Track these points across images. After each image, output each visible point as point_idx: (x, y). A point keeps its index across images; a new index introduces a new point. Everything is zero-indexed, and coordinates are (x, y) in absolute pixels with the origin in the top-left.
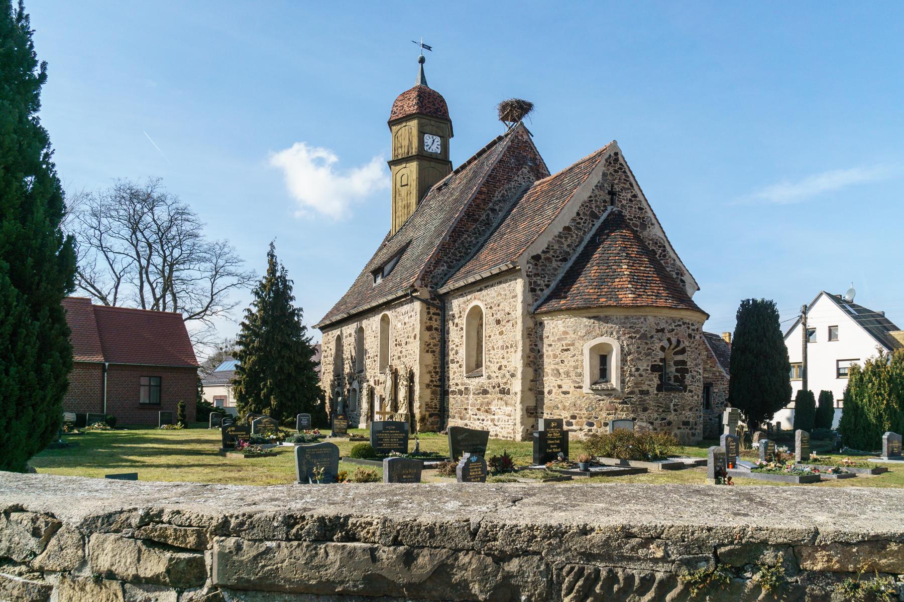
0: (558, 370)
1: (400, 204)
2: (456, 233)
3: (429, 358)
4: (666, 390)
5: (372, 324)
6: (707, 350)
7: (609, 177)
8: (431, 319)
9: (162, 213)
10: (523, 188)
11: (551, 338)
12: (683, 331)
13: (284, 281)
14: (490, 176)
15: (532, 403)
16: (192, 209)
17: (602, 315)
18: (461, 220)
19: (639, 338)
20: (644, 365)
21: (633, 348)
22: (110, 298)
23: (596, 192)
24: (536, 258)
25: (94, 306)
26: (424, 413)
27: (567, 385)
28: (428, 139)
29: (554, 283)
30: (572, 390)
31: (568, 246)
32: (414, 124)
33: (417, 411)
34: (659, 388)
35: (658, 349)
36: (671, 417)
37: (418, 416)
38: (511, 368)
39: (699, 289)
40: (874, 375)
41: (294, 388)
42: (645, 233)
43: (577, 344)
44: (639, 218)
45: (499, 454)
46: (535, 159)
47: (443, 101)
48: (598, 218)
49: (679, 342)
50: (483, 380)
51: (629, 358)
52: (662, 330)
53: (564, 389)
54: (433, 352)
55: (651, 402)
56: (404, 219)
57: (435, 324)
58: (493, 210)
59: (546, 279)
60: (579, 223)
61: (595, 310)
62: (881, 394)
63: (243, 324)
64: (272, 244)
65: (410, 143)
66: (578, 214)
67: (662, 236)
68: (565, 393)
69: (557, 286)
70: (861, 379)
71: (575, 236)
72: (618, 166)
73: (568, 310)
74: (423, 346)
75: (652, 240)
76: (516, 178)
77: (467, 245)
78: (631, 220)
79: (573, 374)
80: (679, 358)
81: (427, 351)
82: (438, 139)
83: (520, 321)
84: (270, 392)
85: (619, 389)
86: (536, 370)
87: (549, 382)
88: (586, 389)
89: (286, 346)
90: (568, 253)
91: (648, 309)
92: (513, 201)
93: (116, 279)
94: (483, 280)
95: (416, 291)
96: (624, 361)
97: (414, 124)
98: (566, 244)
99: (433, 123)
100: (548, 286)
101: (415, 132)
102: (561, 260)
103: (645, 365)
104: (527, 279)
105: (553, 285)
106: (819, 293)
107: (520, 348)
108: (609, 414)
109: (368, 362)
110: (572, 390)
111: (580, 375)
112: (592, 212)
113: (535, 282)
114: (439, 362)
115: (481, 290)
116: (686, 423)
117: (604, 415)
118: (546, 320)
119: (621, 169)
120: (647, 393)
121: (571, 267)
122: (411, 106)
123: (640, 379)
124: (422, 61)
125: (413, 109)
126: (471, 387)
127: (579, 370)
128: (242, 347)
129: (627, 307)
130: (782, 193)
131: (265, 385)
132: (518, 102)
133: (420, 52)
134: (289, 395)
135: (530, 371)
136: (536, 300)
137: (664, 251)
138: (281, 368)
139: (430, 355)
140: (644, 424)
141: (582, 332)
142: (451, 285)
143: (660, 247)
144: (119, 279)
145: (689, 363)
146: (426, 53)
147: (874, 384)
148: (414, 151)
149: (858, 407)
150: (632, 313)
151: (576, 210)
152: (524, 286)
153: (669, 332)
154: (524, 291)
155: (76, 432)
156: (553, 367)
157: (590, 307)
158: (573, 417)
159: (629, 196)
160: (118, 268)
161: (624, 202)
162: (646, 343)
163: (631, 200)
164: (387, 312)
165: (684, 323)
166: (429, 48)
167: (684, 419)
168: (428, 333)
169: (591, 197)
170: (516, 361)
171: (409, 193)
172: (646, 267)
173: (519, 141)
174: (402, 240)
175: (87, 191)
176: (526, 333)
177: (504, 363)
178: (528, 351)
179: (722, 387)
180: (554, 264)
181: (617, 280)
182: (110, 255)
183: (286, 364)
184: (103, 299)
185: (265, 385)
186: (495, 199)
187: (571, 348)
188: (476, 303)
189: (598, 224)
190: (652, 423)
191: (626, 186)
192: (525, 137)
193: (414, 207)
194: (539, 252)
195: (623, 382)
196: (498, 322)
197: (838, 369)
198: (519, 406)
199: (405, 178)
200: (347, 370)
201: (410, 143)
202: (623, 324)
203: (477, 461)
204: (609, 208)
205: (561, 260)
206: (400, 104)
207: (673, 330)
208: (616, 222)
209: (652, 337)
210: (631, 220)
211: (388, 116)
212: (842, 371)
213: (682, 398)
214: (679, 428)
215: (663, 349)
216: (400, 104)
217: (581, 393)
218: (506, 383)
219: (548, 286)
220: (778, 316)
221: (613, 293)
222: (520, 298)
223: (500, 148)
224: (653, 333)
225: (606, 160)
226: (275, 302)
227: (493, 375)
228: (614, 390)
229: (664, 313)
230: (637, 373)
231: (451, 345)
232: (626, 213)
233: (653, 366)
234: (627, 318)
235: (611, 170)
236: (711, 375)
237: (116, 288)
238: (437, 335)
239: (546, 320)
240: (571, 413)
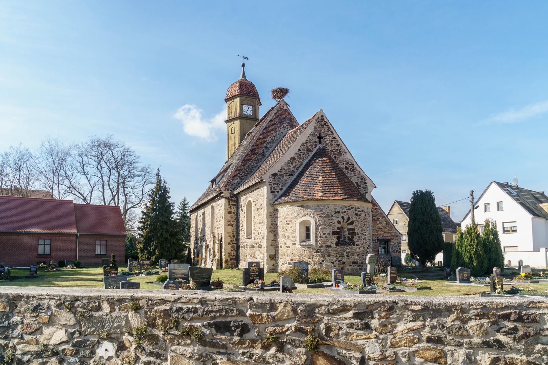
0: (284, 235)
2: (245, 161)
3: (230, 229)
4: (341, 245)
5: (208, 209)
7: (318, 129)
8: (230, 207)
9: (117, 153)
10: (284, 135)
11: (281, 218)
12: (352, 213)
13: (165, 189)
14: (264, 129)
15: (273, 253)
16: (132, 148)
17: (305, 205)
18: (248, 154)
20: (328, 231)
21: (322, 222)
22: (88, 198)
23: (310, 138)
24: (275, 175)
25: (75, 204)
26: (227, 258)
27: (289, 243)
28: (245, 108)
29: (283, 189)
30: (291, 245)
31: (294, 167)
32: (237, 100)
33: (223, 257)
34: (337, 244)
35: (336, 222)
36: (345, 259)
37: (224, 260)
38: (262, 234)
39: (376, 187)
40: (469, 234)
41: (169, 245)
42: (341, 158)
43: (293, 221)
44: (337, 150)
45: (216, 280)
46: (291, 118)
47: (254, 86)
49: (349, 218)
50: (252, 240)
51: (319, 228)
52: (339, 212)
53: (287, 245)
54: (232, 225)
56: (233, 151)
57: (233, 210)
58: (266, 148)
59: (281, 186)
60: (300, 155)
62: (472, 245)
63: (142, 212)
64: (158, 169)
66: (299, 150)
67: (351, 158)
69: (287, 189)
70: (462, 237)
71: (297, 162)
72: (323, 123)
73: (288, 202)
74: (226, 222)
75: (345, 161)
76: (280, 129)
77: (251, 167)
78: (332, 151)
79: (291, 237)
80: (350, 227)
81: (229, 225)
82: (251, 107)
83: (266, 208)
84: (156, 247)
85: (314, 244)
86: (275, 235)
87: (281, 241)
88: (298, 245)
89: (164, 222)
90: (294, 171)
91: (329, 201)
92: (277, 142)
93: (91, 189)
94: (253, 185)
95: (222, 193)
96: (317, 229)
97: (237, 100)
98: (292, 166)
99: (248, 99)
100: (281, 189)
101: (238, 104)
104: (269, 187)
105: (284, 189)
106: (490, 183)
107: (266, 223)
109: (207, 230)
110: (291, 245)
111: (295, 237)
113: (274, 188)
114: (236, 230)
115: (251, 192)
116: (355, 263)
117: (307, 259)
118: (279, 208)
119: (325, 124)
120: (330, 246)
121: (295, 179)
122: (236, 91)
123: (326, 239)
124: (243, 65)
125: (237, 92)
126: (248, 244)
127: (294, 235)
128: (142, 224)
129: (317, 200)
130: (510, 116)
131: (153, 244)
132: (280, 89)
133: (242, 61)
134: (166, 249)
135: (272, 235)
136: (275, 197)
137: (353, 167)
138: (162, 235)
139: (230, 227)
140: (329, 264)
141: (295, 214)
142: (241, 189)
144: (93, 188)
145: (356, 230)
146: (245, 61)
147: (468, 239)
148: (238, 115)
149: (459, 252)
150: (320, 203)
151: (298, 148)
152: (268, 190)
153: (343, 213)
154: (267, 193)
155: (55, 270)
156: (282, 233)
159: (331, 138)
160: (92, 182)
161: (328, 142)
162: (329, 220)
163: (331, 141)
164: (213, 204)
165: (352, 208)
166: (247, 59)
167: (353, 260)
168: (229, 215)
170: (264, 231)
171: (235, 138)
172: (333, 178)
173: (281, 109)
174: (229, 163)
175: (76, 144)
176: (269, 215)
177: (260, 231)
178: (270, 225)
179: (396, 242)
180: (285, 178)
182: (89, 176)
183: (164, 232)
184: (85, 199)
185: (153, 244)
186: (268, 141)
187: (290, 223)
188: (250, 199)
189: (311, 154)
190: (333, 263)
191: (328, 133)
192: (285, 107)
193: (237, 145)
194: (276, 172)
195: (316, 241)
197: (504, 228)
198: (265, 254)
199: (233, 129)
200: (199, 235)
201: (236, 110)
202: (316, 210)
203: (173, 283)
204: (319, 146)
206: (230, 90)
207: (345, 212)
208: (322, 153)
209: (332, 216)
210: (332, 151)
211: (224, 97)
212: (506, 229)
213: (352, 249)
215: (339, 222)
216: (230, 90)
219: (281, 189)
220: (434, 200)
221: (311, 194)
222: (266, 197)
223: (272, 114)
224: (333, 214)
225: (316, 120)
226: (160, 199)
227: (256, 237)
228: (312, 245)
229: (340, 203)
230: (324, 236)
231: (241, 222)
232: (329, 148)
233: (333, 232)
234: (318, 206)
235: (319, 125)
236: (389, 235)
237: (91, 193)
238: (234, 216)
239: (279, 208)
240: (291, 258)
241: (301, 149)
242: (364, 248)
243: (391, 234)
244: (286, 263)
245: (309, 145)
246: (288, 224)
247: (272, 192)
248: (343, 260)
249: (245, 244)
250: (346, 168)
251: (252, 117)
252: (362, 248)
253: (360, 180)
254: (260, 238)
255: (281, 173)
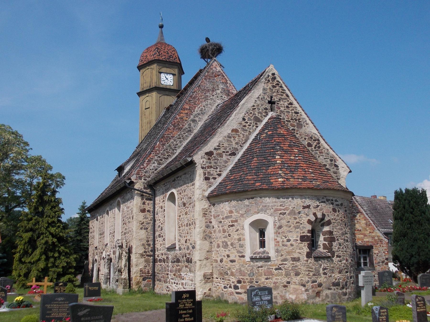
1: (145, 121)
3: (143, 234)
6: (365, 219)
8: (144, 203)
19: (289, 214)
23: (258, 102)
30: (237, 259)
31: (237, 143)
36: (322, 279)
42: (302, 130)
48: (260, 121)
53: (232, 258)
55: (302, 267)
58: (194, 121)
60: (245, 126)
61: (251, 193)
65: (152, 79)
66: (244, 119)
67: (316, 132)
68: (232, 261)
72: (275, 83)
76: (212, 97)
77: (173, 147)
81: (141, 229)
98: (234, 143)
102: (230, 155)
103: (295, 236)
108: (267, 279)
110: (237, 259)
111: (242, 246)
112: (255, 117)
113: (209, 173)
116: (336, 284)
119: (278, 84)
120: (298, 260)
137: (319, 143)
139: (143, 231)
140: (297, 287)
143: (315, 140)
151: (242, 116)
157: (247, 191)
158: (239, 282)
159: (286, 104)
161: (282, 109)
163: (287, 107)
169: (254, 106)
179: (381, 249)
181: (271, 168)
186: (195, 113)
190: (304, 286)
194: (212, 149)
196: (184, 204)
201: (152, 79)
205: (230, 155)
207: (318, 206)
209: (299, 213)
210: (290, 121)
211: (137, 63)
214: (330, 289)
216: (145, 55)
217: (244, 262)
218: (189, 254)
224: (301, 209)
227: (182, 247)
230: (289, 243)
233: (301, 236)
235: (270, 85)
236: (370, 240)
241: (246, 118)
242: (347, 260)
243: (373, 238)
244: (230, 287)
245: (256, 113)
246: (232, 226)
247: (207, 179)
248: (319, 280)
249: (164, 257)
250: (309, 145)
251: (172, 88)
252: (344, 261)
253: (329, 162)
254: (188, 248)
255: (219, 151)
